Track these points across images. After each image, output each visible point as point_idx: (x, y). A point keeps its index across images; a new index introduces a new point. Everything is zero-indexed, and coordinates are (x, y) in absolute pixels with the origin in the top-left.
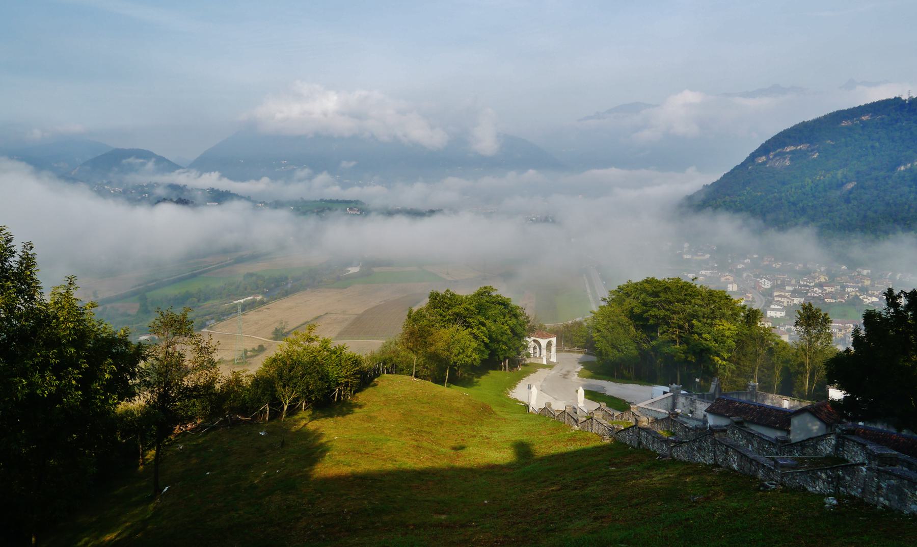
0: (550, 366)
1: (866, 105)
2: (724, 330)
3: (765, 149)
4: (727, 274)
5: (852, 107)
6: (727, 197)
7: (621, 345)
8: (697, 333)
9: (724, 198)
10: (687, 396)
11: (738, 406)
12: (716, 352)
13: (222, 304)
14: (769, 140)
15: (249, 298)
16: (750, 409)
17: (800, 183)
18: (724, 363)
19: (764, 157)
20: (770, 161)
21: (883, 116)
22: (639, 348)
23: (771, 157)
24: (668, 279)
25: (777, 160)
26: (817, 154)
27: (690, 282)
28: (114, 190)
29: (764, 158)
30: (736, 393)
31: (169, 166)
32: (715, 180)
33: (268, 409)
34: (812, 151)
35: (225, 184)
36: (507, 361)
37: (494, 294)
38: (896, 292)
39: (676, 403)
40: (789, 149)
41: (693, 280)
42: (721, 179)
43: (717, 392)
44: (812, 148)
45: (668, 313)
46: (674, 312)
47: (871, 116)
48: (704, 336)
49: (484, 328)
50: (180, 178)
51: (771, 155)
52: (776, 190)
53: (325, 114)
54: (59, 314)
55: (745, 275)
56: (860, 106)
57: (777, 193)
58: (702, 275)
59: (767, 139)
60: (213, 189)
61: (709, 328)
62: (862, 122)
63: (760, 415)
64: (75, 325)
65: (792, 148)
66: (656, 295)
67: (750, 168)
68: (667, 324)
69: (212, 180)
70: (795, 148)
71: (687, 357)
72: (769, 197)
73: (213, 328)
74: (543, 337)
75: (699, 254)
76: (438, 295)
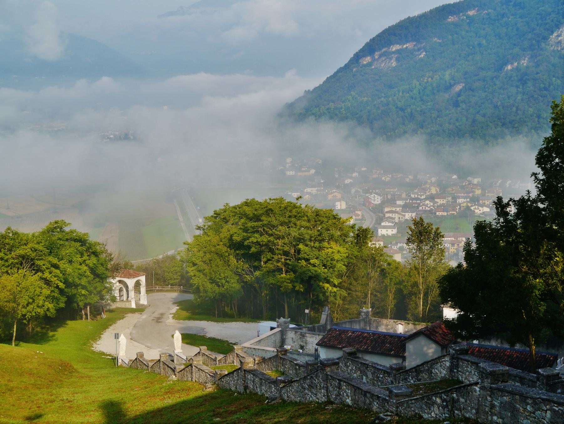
0: (140, 309)
2: (333, 253)
4: (334, 190)
6: (331, 103)
7: (220, 279)
8: (304, 259)
9: (328, 105)
10: (295, 330)
11: (351, 335)
12: (325, 279)
14: (374, 39)
16: (364, 338)
18: (335, 289)
20: (376, 62)
21: (490, 11)
22: (241, 280)
23: (376, 57)
24: (270, 199)
29: (368, 59)
32: (317, 85)
34: (419, 50)
36: (88, 308)
37: (67, 229)
39: (285, 339)
40: (395, 48)
41: (297, 199)
43: (328, 323)
44: (419, 46)
45: (271, 239)
47: (478, 11)
55: (353, 191)
59: (372, 38)
61: (317, 253)
62: (468, 17)
63: (374, 343)
66: (257, 218)
67: (354, 70)
68: (271, 251)
70: (401, 47)
71: (294, 287)
74: (130, 276)
75: (303, 169)
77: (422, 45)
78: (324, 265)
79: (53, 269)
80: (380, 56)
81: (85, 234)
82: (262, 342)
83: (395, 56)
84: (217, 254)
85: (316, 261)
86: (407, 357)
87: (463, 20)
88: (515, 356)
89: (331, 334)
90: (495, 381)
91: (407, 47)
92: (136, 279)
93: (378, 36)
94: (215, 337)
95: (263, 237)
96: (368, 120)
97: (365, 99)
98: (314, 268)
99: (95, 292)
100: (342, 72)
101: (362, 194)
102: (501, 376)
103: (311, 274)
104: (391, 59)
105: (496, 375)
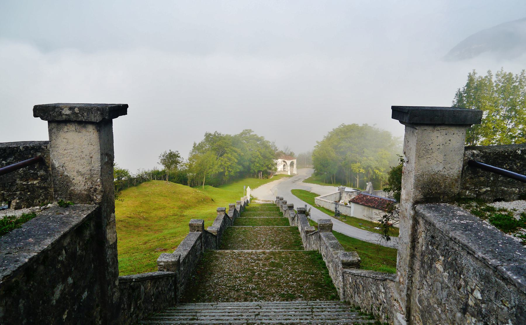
8: (366, 157)
16: (375, 200)
27: (372, 126)
37: (252, 133)
43: (371, 190)
48: (369, 158)
49: (235, 154)
54: (418, 291)
64: (508, 161)
76: (210, 134)
78: (377, 161)
82: (328, 197)
85: (372, 158)
92: (291, 161)
94: (314, 192)
98: (370, 162)
99: (265, 165)
102: (196, 227)
103: (368, 164)
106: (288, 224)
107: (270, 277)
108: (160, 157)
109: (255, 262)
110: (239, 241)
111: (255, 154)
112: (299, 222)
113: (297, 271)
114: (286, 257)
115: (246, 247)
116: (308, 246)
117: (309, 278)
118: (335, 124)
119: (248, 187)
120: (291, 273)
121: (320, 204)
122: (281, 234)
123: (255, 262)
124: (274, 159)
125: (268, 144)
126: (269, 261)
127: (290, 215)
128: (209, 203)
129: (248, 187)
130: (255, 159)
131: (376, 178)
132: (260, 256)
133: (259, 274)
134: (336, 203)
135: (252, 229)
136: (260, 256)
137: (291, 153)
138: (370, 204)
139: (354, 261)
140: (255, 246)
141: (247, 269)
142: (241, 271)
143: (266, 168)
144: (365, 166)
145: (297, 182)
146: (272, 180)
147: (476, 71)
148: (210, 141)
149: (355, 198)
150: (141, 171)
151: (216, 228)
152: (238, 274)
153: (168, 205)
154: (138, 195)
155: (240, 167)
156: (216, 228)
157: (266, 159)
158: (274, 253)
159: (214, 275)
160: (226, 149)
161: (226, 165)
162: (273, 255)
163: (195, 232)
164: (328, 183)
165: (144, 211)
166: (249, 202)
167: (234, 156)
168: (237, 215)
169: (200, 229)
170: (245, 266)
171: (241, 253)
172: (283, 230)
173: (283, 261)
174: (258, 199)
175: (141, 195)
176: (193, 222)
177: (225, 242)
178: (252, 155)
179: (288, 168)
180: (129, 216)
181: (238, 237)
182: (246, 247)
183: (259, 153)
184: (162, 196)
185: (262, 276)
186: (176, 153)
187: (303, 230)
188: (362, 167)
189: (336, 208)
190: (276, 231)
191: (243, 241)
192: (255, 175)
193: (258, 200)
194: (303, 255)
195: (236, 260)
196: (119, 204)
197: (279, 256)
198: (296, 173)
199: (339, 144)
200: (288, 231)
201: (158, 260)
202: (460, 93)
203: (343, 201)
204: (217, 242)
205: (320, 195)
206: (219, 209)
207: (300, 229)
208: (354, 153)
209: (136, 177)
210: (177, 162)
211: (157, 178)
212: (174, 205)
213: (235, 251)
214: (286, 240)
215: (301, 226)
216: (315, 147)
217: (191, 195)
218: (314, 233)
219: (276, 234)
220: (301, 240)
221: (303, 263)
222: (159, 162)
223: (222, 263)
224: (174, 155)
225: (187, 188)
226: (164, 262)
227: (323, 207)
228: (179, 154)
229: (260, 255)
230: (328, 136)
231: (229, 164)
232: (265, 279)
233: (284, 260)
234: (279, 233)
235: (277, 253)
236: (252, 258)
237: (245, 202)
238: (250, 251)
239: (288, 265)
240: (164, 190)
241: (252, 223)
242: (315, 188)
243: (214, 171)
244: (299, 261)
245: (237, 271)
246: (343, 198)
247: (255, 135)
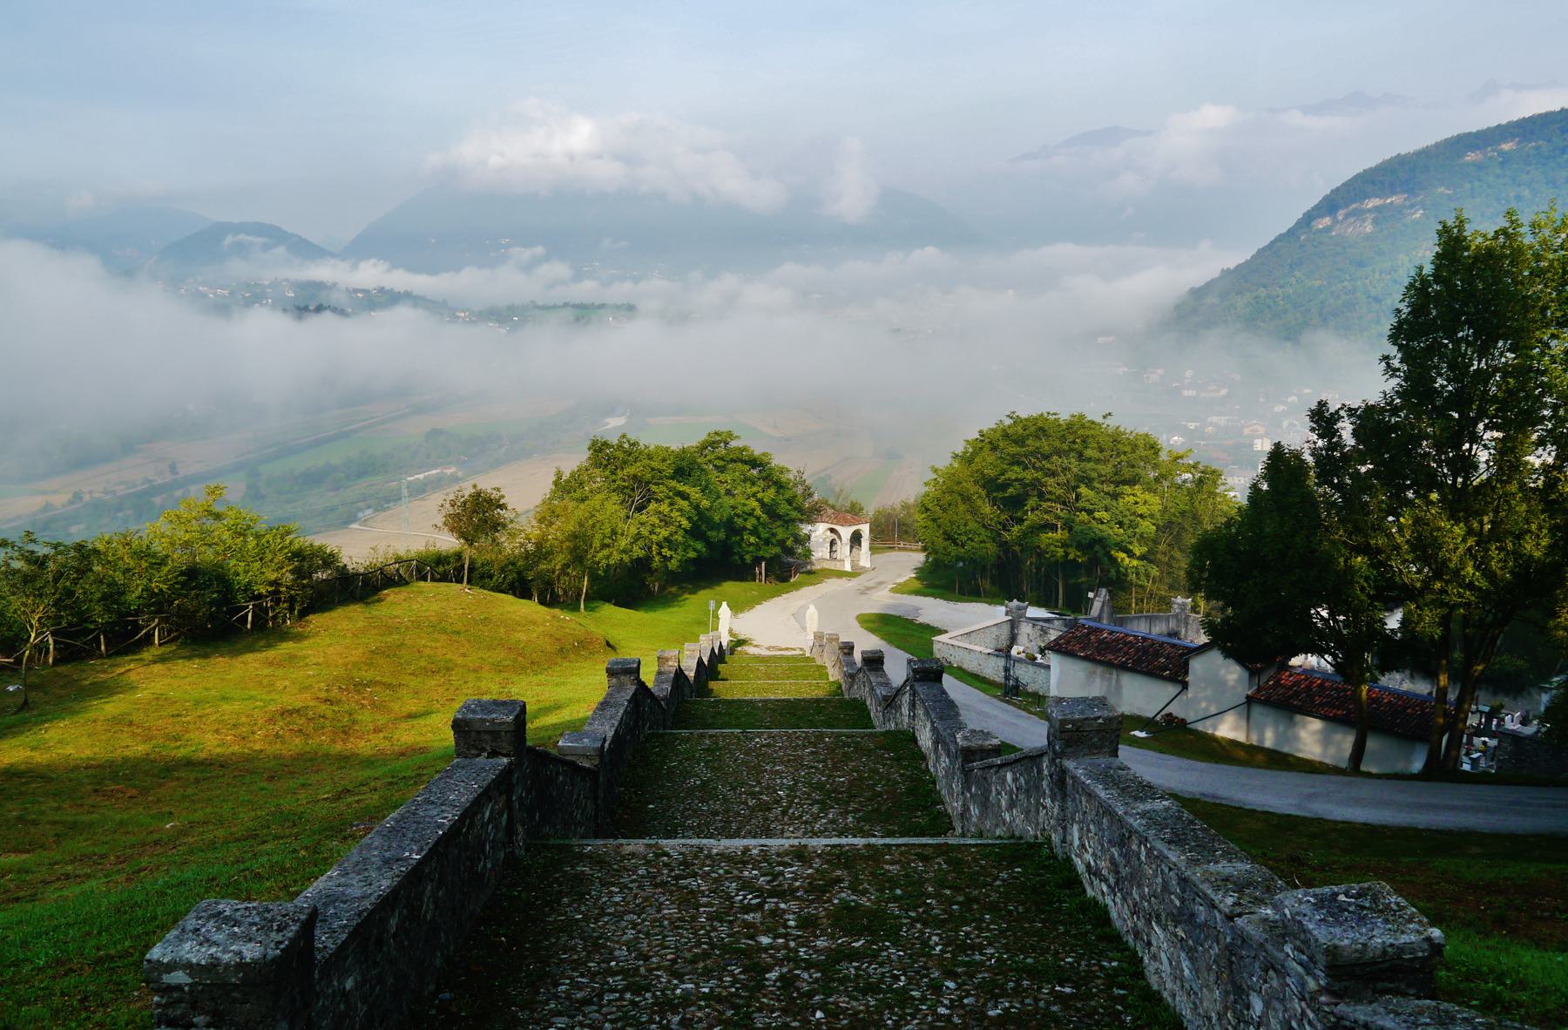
0: (856, 573)
1: (1509, 123)
2: (1136, 503)
3: (1329, 205)
5: (1485, 127)
6: (1262, 289)
8: (1086, 511)
12: (1117, 544)
13: (387, 482)
14: (1338, 189)
15: (434, 472)
16: (1126, 644)
17: (1390, 264)
18: (1135, 563)
19: (1328, 218)
20: (1339, 226)
21: (1540, 142)
22: (996, 537)
23: (1340, 218)
25: (1351, 224)
26: (1421, 212)
27: (1099, 420)
28: (215, 294)
29: (1327, 221)
30: (1146, 617)
31: (306, 250)
33: (51, 641)
34: (1412, 206)
35: (399, 280)
36: (763, 564)
37: (733, 444)
38: (1333, 407)
39: (1017, 634)
40: (1372, 203)
41: (1104, 417)
42: (1252, 257)
43: (1105, 615)
44: (1413, 201)
45: (1039, 475)
46: (1053, 474)
47: (1518, 143)
48: (1097, 515)
49: (684, 504)
50: (322, 272)
51: (1341, 214)
52: (1347, 277)
53: (572, 157)
55: (1285, 424)
56: (1499, 126)
57: (1349, 281)
58: (1211, 424)
59: (1334, 187)
60: (383, 288)
61: (1108, 501)
62: (1501, 153)
65: (1377, 202)
67: (1302, 237)
68: (1041, 496)
69: (370, 274)
70: (1382, 202)
71: (1067, 554)
72: (1334, 288)
73: (369, 523)
74: (845, 523)
75: (1211, 388)
76: (605, 444)
77: (1419, 199)
78: (1121, 524)
79: (678, 499)
80: (1347, 216)
81: (764, 454)
83: (1371, 216)
84: (961, 495)
86: (1190, 683)
87: (1491, 158)
88: (1386, 701)
89: (1073, 633)
90: (468, 749)
91: (1392, 202)
92: (854, 528)
93: (1345, 185)
95: (1027, 471)
96: (1320, 315)
97: (1317, 283)
99: (774, 541)
100: (1281, 241)
101: (1299, 428)
102: (487, 737)
104: (1364, 221)
105: (473, 734)
106: (868, 723)
107: (843, 1002)
108: (442, 506)
109: (760, 906)
110: (691, 790)
111: (744, 505)
112: (920, 712)
113: (978, 957)
114: (907, 876)
115: (717, 813)
116: (975, 811)
117: (1048, 1004)
118: (989, 416)
119: (724, 604)
120: (952, 975)
121: (952, 659)
122: (852, 761)
123: (760, 906)
124: (802, 521)
125: (784, 478)
126: (829, 900)
127: (872, 689)
128: (596, 656)
129: (724, 604)
130: (745, 520)
131: (1118, 578)
132: (782, 873)
133: (787, 982)
134: (1004, 652)
135: (739, 739)
136: (782, 873)
137: (853, 505)
138: (1110, 657)
139: (1401, 949)
140: (752, 809)
141: (725, 948)
142: (694, 961)
143: (777, 550)
144: (1083, 541)
145: (873, 591)
146: (798, 586)
147: (1465, 215)
148: (606, 466)
149: (1060, 638)
150: (381, 552)
151: (595, 740)
152: (680, 977)
153: (460, 660)
154: (364, 627)
155: (699, 546)
156: (595, 740)
157: (778, 523)
158: (847, 859)
159: (557, 985)
160: (653, 488)
161: (654, 537)
162: (847, 867)
163: (482, 760)
164: (969, 595)
165: (378, 678)
166: (727, 653)
167: (680, 510)
168: (687, 691)
169: (506, 746)
170: (714, 929)
171: (696, 857)
172: (858, 743)
173: (896, 899)
174: (755, 643)
175: (374, 627)
176: (474, 712)
177: (635, 793)
178: (733, 508)
179: (843, 549)
180: (323, 695)
181: (687, 774)
182: (717, 813)
183: (755, 504)
184: (444, 631)
185: (801, 995)
186: (495, 495)
187: (945, 744)
188: (1074, 544)
189: (1007, 670)
190: (833, 750)
191: (706, 791)
192: (743, 572)
193: (756, 646)
194: (982, 867)
195: (671, 893)
196: (296, 657)
197: (872, 874)
198: (868, 565)
199: (1003, 474)
200: (881, 749)
201: (156, 953)
202: (1422, 280)
203: (1021, 649)
204: (601, 794)
205: (946, 632)
206: (617, 663)
207: (925, 739)
208: (1049, 500)
209: (362, 571)
210: (497, 526)
211: (432, 574)
212: (482, 658)
213: (667, 844)
214: (876, 785)
215: (934, 730)
216: (926, 484)
217: (541, 629)
218: (1016, 761)
219: (832, 759)
220: (934, 783)
221: (993, 908)
222: (440, 525)
223: (603, 913)
224: (489, 501)
225: (530, 608)
226: (189, 967)
227: (959, 668)
228: (503, 497)
229: (786, 865)
230: (965, 453)
231: (664, 533)
232: (819, 1014)
233: (898, 892)
234: (844, 754)
235: (862, 857)
236: (747, 885)
237: (713, 649)
238: (737, 844)
239: (925, 924)
240: (453, 613)
241: (737, 718)
242: (932, 610)
243: (616, 557)
244: (976, 900)
245: (674, 961)
246: (1022, 638)
247: (745, 449)
